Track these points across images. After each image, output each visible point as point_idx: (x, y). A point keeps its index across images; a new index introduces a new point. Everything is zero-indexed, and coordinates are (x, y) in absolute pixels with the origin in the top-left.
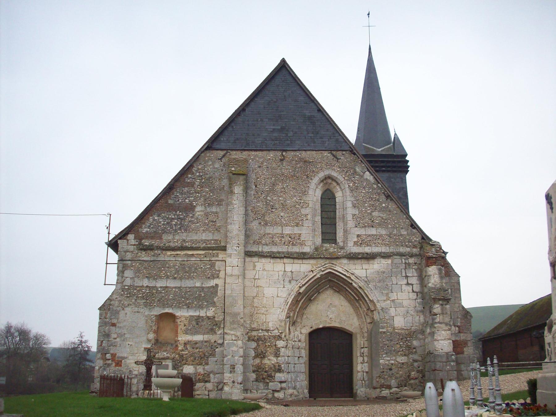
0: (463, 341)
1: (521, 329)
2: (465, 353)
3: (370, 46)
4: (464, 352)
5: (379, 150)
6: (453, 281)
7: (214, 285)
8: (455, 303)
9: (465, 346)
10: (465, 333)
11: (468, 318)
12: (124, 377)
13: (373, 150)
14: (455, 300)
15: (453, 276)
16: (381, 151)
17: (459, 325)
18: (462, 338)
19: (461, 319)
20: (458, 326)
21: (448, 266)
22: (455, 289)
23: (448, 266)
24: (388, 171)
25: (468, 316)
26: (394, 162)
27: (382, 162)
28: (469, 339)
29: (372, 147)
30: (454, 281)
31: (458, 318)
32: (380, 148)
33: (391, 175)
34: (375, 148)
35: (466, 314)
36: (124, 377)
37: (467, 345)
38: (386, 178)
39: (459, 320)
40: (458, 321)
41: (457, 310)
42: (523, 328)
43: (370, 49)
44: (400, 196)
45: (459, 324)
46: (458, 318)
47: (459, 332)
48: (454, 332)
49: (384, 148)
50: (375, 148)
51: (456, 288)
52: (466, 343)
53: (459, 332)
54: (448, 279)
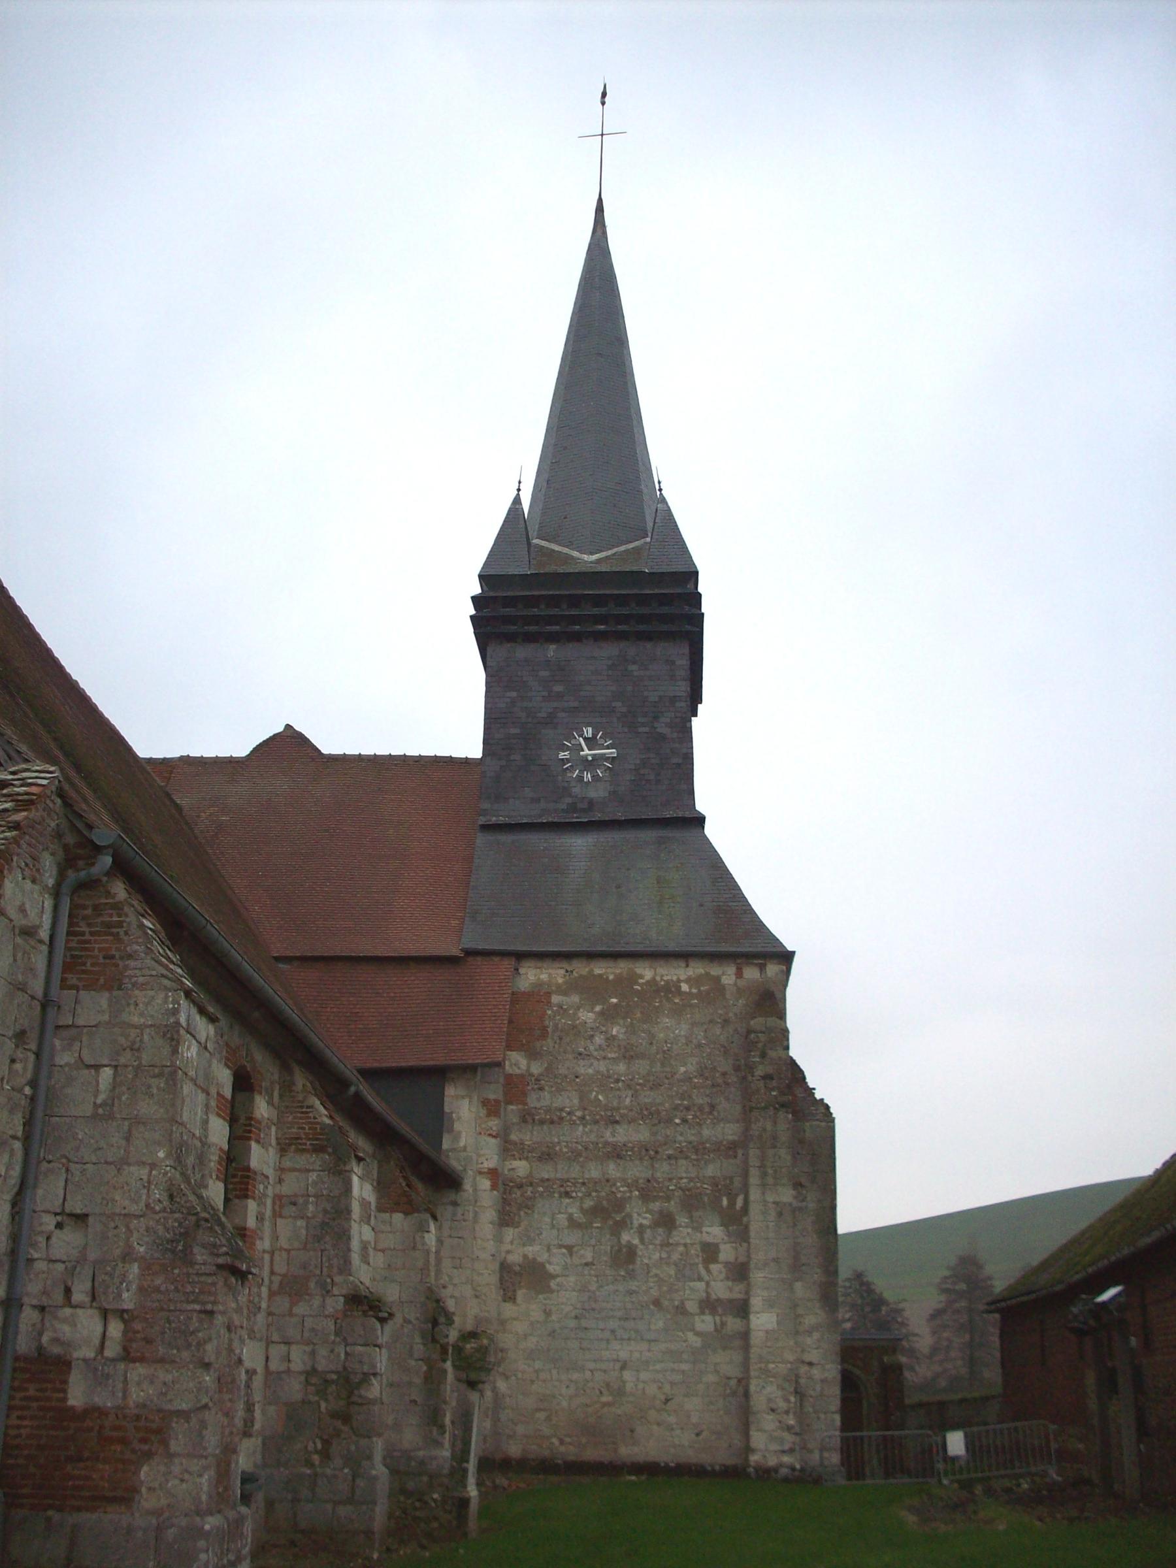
0: (138, 1417)
1: (1148, 1240)
2: (147, 1501)
3: (600, 201)
4: (135, 1490)
5: (589, 559)
6: (135, 1019)
7: (751, 1133)
8: (125, 1161)
9: (149, 1455)
10: (162, 1361)
11: (192, 1264)
12: (217, 1414)
13: (568, 559)
14: (128, 1138)
15: (142, 987)
16: (598, 561)
17: (126, 1306)
18: (136, 1395)
19: (147, 1267)
20: (121, 1313)
21: (120, 924)
22: (138, 1069)
23: (120, 924)
24: (621, 636)
25: (196, 1250)
26: (643, 600)
27: (599, 601)
28: (184, 1406)
29: (566, 550)
30: (142, 1015)
31: (128, 1256)
32: (592, 554)
33: (631, 649)
34: (575, 554)
35: (185, 1235)
36: (217, 1414)
37: (165, 1443)
38: (610, 662)
39: (135, 1269)
40: (124, 1277)
41: (134, 1209)
42: (1156, 1235)
43: (600, 209)
44: (662, 729)
45: (128, 1300)
46: (128, 1256)
47: (127, 1356)
48: (91, 1354)
49: (615, 550)
50: (575, 554)
51: (146, 1058)
52: (158, 1431)
53: (127, 1356)
54: (104, 1003)
